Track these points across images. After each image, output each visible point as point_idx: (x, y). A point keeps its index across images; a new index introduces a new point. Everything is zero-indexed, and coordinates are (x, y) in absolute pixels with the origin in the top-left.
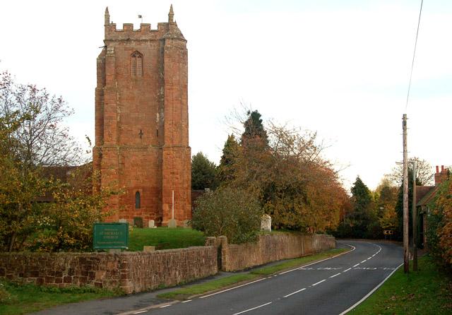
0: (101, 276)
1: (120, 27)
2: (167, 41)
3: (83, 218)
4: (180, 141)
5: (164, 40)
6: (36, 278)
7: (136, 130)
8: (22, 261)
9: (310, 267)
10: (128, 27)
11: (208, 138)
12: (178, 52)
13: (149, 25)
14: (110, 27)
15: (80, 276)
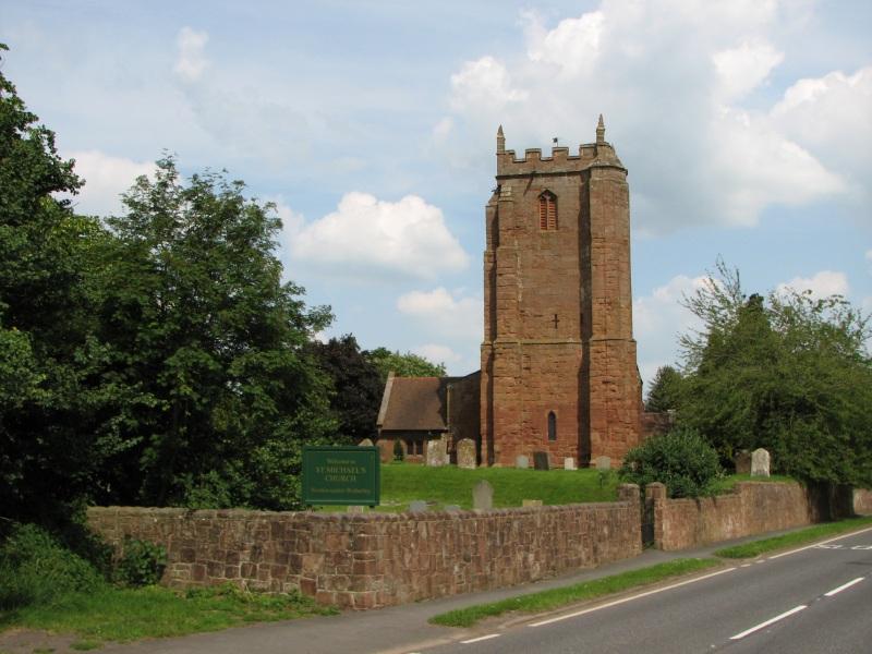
0: (313, 564)
1: (520, 155)
2: (593, 173)
3: (663, 465)
4: (618, 331)
5: (589, 171)
6: (190, 565)
7: (548, 316)
8: (166, 527)
9: (836, 543)
10: (534, 153)
11: (664, 329)
12: (611, 188)
13: (565, 150)
14: (505, 155)
15: (272, 563)
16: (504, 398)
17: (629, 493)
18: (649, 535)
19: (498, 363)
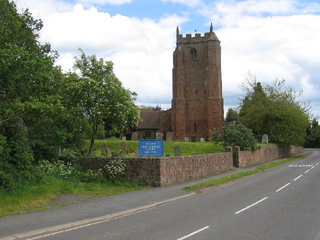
1: (184, 36)
2: (209, 43)
14: (179, 36)
16: (180, 118)
17: (229, 150)
18: (236, 164)
19: (178, 106)
